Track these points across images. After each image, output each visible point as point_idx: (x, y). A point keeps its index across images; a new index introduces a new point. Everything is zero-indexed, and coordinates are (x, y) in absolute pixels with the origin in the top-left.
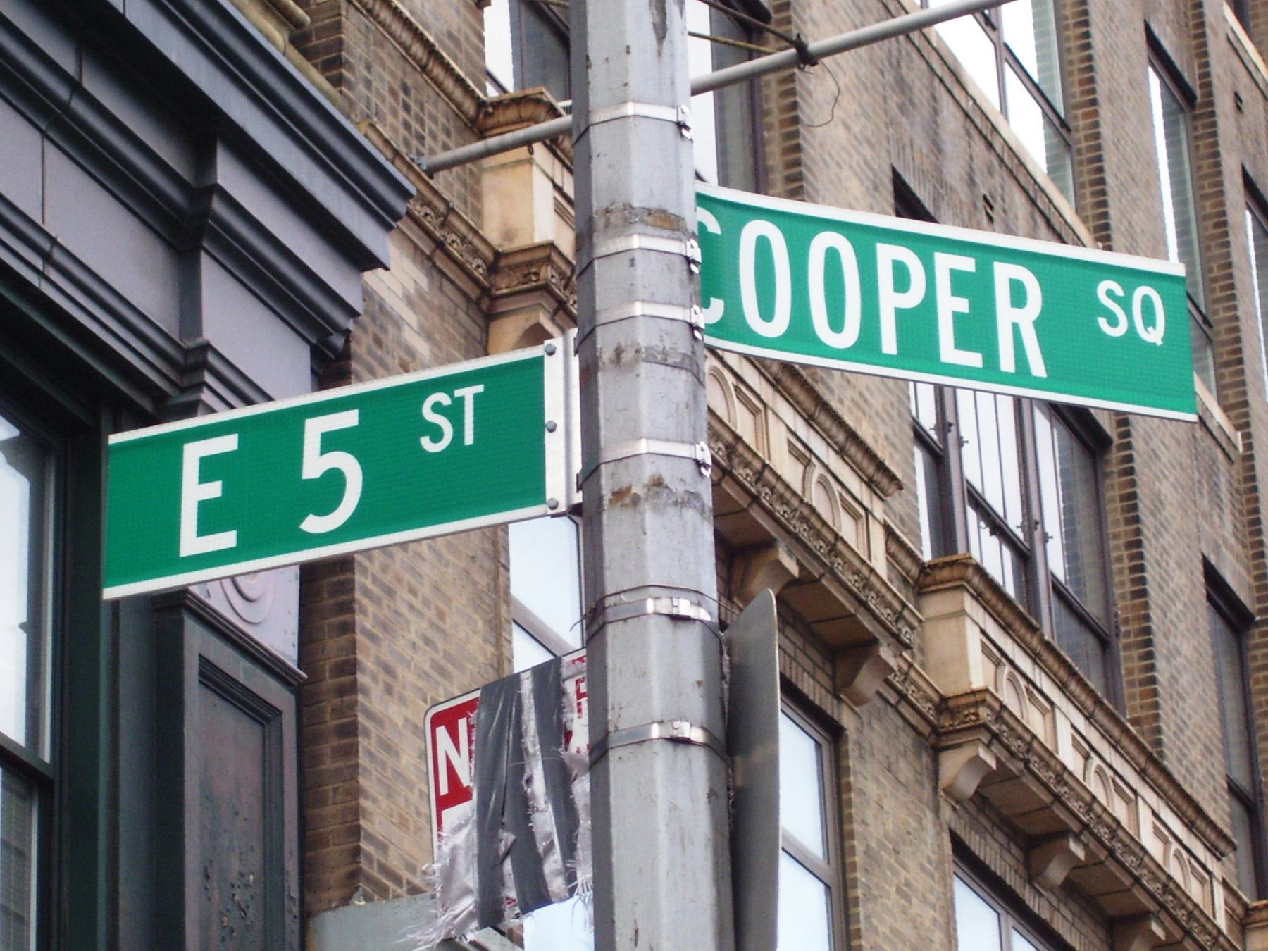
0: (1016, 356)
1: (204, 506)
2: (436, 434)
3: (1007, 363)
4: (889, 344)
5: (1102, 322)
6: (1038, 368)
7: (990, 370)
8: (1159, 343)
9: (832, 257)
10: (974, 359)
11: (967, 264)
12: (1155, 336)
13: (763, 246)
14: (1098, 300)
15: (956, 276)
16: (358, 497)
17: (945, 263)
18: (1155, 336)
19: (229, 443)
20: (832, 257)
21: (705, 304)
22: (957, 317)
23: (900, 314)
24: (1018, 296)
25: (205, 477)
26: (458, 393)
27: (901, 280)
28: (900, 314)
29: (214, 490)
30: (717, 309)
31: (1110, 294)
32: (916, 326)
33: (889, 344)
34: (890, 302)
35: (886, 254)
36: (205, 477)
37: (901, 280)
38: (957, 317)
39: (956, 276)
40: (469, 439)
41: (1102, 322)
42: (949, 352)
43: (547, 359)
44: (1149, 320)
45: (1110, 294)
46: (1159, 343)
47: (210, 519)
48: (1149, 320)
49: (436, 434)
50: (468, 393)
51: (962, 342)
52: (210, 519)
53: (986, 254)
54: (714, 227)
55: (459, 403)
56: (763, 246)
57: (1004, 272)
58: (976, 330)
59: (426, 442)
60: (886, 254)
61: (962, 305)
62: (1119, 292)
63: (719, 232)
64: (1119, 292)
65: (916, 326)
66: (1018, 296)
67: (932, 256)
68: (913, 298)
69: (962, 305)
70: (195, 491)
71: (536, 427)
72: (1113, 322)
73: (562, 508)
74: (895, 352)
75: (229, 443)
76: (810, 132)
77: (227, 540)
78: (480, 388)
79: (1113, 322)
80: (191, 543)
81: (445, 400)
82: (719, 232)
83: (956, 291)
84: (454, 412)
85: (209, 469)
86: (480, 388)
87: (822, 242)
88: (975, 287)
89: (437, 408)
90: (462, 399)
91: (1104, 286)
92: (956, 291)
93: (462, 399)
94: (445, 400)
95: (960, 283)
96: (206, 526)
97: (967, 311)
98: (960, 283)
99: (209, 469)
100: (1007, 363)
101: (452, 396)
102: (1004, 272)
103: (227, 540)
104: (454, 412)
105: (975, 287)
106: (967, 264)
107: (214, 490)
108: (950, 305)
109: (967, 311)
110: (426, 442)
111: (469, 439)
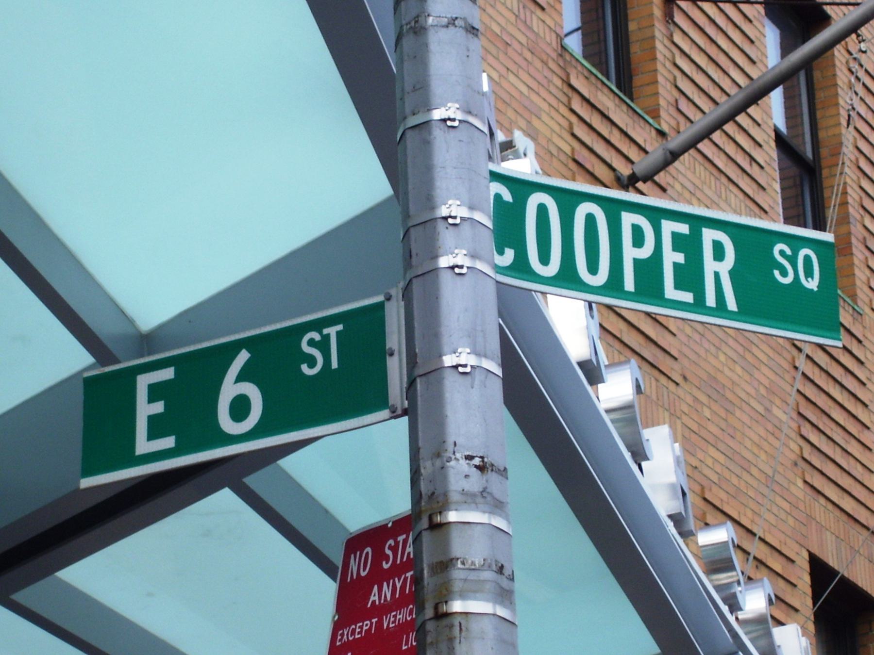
0: (716, 287)
1: (152, 420)
2: (311, 361)
3: (711, 300)
4: (629, 285)
5: (776, 273)
6: (732, 305)
7: (699, 304)
8: (816, 289)
9: (590, 220)
10: (688, 297)
11: (683, 228)
12: (812, 284)
13: (542, 210)
14: (772, 253)
15: (675, 236)
16: (260, 412)
17: (669, 227)
18: (812, 284)
19: (168, 374)
20: (590, 220)
21: (501, 252)
22: (675, 265)
23: (636, 262)
24: (719, 253)
25: (151, 399)
26: (326, 331)
27: (638, 239)
28: (636, 262)
29: (159, 407)
30: (509, 256)
31: (782, 253)
32: (649, 270)
33: (629, 285)
34: (630, 253)
35: (628, 219)
36: (151, 399)
37: (638, 239)
38: (675, 265)
39: (675, 236)
40: (335, 365)
41: (776, 273)
42: (670, 292)
43: (388, 305)
44: (809, 274)
45: (782, 253)
46: (816, 289)
47: (156, 428)
48: (809, 274)
49: (311, 361)
50: (332, 331)
51: (678, 286)
52: (156, 428)
53: (697, 222)
54: (507, 197)
55: (326, 338)
56: (542, 210)
57: (709, 235)
58: (690, 276)
59: (305, 368)
60: (628, 219)
61: (680, 258)
62: (788, 252)
63: (511, 200)
64: (788, 252)
65: (649, 270)
66: (719, 253)
67: (660, 223)
68: (646, 252)
69: (680, 258)
70: (146, 410)
71: (383, 353)
72: (784, 274)
73: (399, 412)
74: (633, 290)
75: (168, 374)
76: (545, 298)
77: (168, 442)
78: (340, 327)
79: (784, 274)
80: (143, 445)
81: (316, 336)
82: (511, 200)
83: (676, 248)
84: (323, 345)
85: (155, 392)
86: (340, 327)
87: (584, 209)
88: (689, 245)
89: (311, 343)
90: (328, 335)
91: (779, 247)
92: (676, 248)
93: (328, 335)
94: (316, 336)
95: (676, 237)
96: (152, 435)
97: (688, 233)
98: (679, 242)
99: (155, 392)
100: (711, 300)
101: (321, 333)
102: (709, 235)
103: (168, 442)
104: (323, 345)
105: (689, 245)
106: (683, 228)
107: (159, 407)
108: (671, 257)
109: (688, 233)
110: (305, 368)
111: (335, 365)
